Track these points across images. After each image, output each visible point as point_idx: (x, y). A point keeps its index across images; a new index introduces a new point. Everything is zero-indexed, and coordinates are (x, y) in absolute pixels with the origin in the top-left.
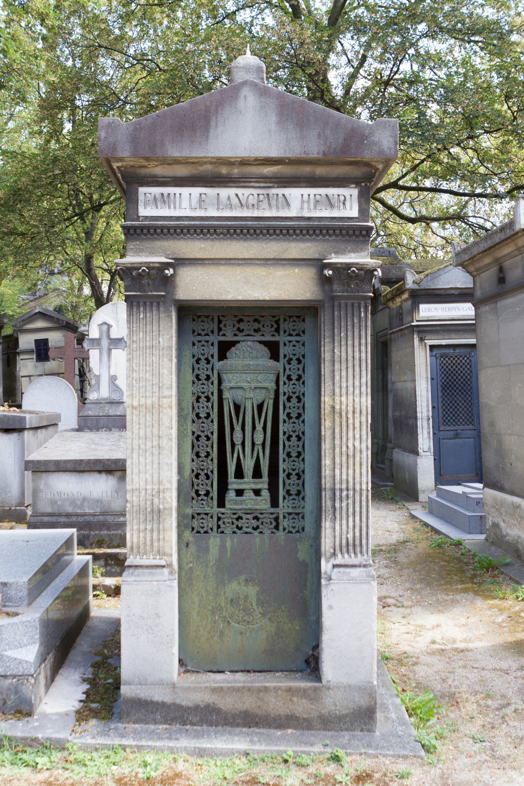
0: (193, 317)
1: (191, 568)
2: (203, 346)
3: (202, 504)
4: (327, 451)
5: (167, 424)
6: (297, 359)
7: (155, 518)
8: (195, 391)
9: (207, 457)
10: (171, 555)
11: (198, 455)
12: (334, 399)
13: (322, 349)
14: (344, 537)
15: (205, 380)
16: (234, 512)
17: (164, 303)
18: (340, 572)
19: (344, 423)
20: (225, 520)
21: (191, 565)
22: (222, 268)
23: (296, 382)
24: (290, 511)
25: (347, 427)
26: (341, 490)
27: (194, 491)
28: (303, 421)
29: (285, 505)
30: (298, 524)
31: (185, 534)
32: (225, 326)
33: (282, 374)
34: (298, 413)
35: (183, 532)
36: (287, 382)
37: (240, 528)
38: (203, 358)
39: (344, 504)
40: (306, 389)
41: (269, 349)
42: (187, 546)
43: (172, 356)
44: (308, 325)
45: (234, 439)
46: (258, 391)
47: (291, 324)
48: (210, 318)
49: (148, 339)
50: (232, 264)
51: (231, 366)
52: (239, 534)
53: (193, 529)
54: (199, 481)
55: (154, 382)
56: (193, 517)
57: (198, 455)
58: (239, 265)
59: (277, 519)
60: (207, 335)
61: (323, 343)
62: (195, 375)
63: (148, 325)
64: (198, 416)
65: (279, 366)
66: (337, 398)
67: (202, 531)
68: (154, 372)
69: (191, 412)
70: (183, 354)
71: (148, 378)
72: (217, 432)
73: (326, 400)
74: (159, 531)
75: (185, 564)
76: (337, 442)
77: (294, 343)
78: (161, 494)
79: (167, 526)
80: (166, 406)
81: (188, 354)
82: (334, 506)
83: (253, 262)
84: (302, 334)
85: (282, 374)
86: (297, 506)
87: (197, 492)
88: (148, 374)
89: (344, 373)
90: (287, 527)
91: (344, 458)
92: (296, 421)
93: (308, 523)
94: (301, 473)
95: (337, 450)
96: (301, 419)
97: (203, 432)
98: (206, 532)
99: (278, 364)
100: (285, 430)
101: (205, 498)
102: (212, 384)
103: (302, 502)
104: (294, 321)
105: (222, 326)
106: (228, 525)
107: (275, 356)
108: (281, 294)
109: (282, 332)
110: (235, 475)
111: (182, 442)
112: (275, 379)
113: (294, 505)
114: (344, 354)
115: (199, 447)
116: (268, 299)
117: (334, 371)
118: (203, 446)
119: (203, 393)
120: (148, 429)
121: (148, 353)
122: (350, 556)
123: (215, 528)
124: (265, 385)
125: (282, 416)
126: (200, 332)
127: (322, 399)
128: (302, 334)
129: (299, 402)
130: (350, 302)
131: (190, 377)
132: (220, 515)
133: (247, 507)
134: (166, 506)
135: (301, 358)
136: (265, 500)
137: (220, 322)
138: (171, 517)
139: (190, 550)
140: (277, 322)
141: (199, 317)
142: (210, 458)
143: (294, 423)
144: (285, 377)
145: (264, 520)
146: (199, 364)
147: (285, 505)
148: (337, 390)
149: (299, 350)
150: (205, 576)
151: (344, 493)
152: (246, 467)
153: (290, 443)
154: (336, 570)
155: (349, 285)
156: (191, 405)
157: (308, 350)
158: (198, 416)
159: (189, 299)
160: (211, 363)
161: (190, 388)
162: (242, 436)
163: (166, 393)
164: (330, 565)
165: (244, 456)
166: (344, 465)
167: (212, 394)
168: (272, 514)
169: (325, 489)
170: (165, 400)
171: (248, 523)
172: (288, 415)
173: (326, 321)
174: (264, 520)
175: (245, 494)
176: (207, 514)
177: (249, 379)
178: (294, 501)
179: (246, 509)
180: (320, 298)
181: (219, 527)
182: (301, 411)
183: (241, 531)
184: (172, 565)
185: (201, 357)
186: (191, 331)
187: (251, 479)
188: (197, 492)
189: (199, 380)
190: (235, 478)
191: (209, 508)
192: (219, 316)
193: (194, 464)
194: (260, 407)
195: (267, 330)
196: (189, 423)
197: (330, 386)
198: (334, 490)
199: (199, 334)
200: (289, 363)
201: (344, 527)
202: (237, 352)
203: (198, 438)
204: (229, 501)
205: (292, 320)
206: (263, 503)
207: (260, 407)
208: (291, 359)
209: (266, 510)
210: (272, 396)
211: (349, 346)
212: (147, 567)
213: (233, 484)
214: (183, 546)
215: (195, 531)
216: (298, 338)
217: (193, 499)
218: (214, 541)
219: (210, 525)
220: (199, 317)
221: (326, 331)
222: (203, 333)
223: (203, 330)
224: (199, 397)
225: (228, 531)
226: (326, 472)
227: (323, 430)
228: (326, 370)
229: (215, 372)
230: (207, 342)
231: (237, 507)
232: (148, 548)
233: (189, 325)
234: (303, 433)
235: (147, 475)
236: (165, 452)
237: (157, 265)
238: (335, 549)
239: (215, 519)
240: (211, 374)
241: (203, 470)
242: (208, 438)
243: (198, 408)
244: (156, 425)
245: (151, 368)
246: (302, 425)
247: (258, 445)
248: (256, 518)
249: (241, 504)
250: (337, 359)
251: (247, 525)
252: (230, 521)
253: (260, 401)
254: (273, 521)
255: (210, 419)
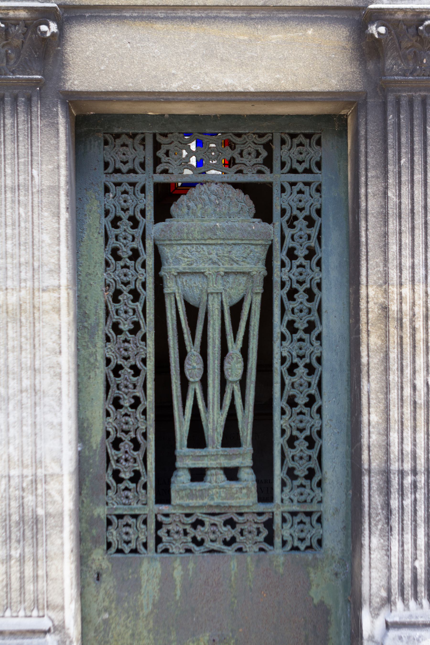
0: (103, 132)
1: (106, 622)
2: (125, 192)
3: (127, 497)
4: (372, 396)
5: (50, 344)
6: (306, 218)
7: (28, 534)
8: (110, 280)
9: (134, 406)
10: (63, 608)
11: (117, 403)
12: (386, 292)
13: (363, 191)
14: (408, 567)
15: (130, 258)
16: (188, 511)
17: (41, 98)
18: (400, 638)
19: (407, 340)
20: (170, 527)
21: (106, 616)
22: (159, 26)
23: (304, 262)
24: (295, 508)
25: (414, 347)
26: (402, 473)
27: (110, 472)
28: (319, 337)
29: (286, 498)
30: (311, 533)
31: (94, 556)
32: (167, 154)
33: (277, 246)
34: (309, 322)
35: (90, 552)
36: (287, 261)
37: (199, 543)
38: (125, 216)
39: (408, 502)
40: (323, 275)
41: (251, 198)
42: (98, 579)
43: (59, 207)
44: (327, 151)
45: (187, 373)
46: (231, 279)
47: (295, 150)
48: (139, 138)
49: (9, 171)
50: (180, 18)
51: (180, 231)
52: (197, 554)
53: (109, 545)
54: (121, 454)
55: (22, 260)
56: (109, 523)
57: (117, 403)
58: (193, 20)
59: (269, 524)
60: (133, 171)
61: (363, 179)
62: (109, 248)
63: (8, 142)
64: (116, 328)
65: (273, 231)
66: (393, 290)
67: (127, 549)
68: (23, 239)
69: (103, 320)
70: (87, 207)
71: (10, 251)
72: (153, 359)
73: (371, 293)
74: (36, 560)
75: (94, 613)
76: (394, 377)
77: (300, 186)
78: (39, 486)
79: (53, 549)
80: (47, 307)
81: (95, 206)
82: (388, 505)
83: (223, 13)
84: (315, 169)
85: (277, 246)
86: (309, 500)
87: (116, 474)
88: (9, 242)
89: (406, 239)
90: (289, 539)
91: (408, 410)
92: (306, 336)
93: (332, 532)
94: (315, 436)
95: (394, 395)
96: (315, 333)
97: (126, 358)
98: (134, 551)
99: (271, 226)
100: (285, 354)
101: (132, 486)
102: (144, 265)
103: (317, 491)
104: (301, 144)
105: (161, 154)
106: (176, 536)
107: (264, 213)
108: (278, 80)
109: (277, 165)
110: (188, 440)
111: (85, 378)
112: (264, 257)
113: (303, 498)
114: (406, 201)
115: (118, 389)
116: (252, 90)
117: (386, 235)
118: (126, 387)
119: (126, 284)
120: (11, 355)
121: (9, 200)
122: (421, 604)
123: (151, 544)
124: (246, 267)
125: (278, 327)
126: (119, 165)
127: (363, 291)
128: (315, 169)
129: (311, 299)
130: (418, 95)
131: (99, 253)
132: (160, 518)
133: (212, 503)
134: (51, 509)
135: (314, 216)
136: (247, 488)
137: (157, 146)
138: (62, 532)
139: (103, 585)
140: (268, 147)
141: (117, 136)
142: (140, 409)
143: (301, 340)
144: (285, 253)
145: (246, 527)
146: (117, 227)
147: (286, 498)
148: (393, 274)
149: (310, 201)
150: (133, 635)
151: (408, 480)
152: (210, 426)
153: (294, 379)
154: (393, 633)
155: (417, 58)
156: (103, 307)
157: (327, 200)
158: (116, 328)
159: (92, 89)
160: (141, 225)
161: (100, 275)
162: (201, 366)
163: (49, 281)
164: (380, 623)
165: (206, 405)
166: (408, 423)
167: (144, 285)
168: (260, 514)
169: (369, 471)
170: (46, 296)
171: (214, 533)
172: (291, 326)
173: (370, 135)
174: (246, 527)
175: (208, 478)
176: (135, 516)
177: (214, 256)
178: (302, 489)
179: (211, 506)
180: (358, 87)
181: (158, 540)
182: (314, 317)
183: (202, 549)
184: (64, 627)
185: (121, 214)
186: (102, 165)
187: (220, 449)
188: (116, 474)
189: (118, 258)
190: (189, 446)
191: (140, 505)
192: (155, 135)
193: (110, 420)
194: (236, 310)
195: (249, 160)
196: (100, 341)
197: (377, 265)
198: (386, 473)
199: (117, 171)
200: (292, 226)
201: (408, 546)
202: (191, 204)
203: (117, 370)
204: (178, 492)
205: (296, 141)
206: (243, 494)
207: (236, 310)
208: (295, 218)
209: (248, 507)
210: (260, 289)
211: (416, 185)
212: (13, 634)
213: (187, 458)
214: (91, 578)
215: (113, 550)
216: (308, 177)
217: (108, 487)
218: (150, 569)
219: (143, 539)
220: (117, 136)
221: (371, 154)
222: (125, 168)
223: (125, 163)
224: (117, 294)
225: (177, 548)
226: (371, 437)
227: (364, 353)
228: (370, 233)
229: (149, 244)
230: (133, 184)
231: (193, 502)
232: (15, 595)
233: (97, 152)
234: (319, 360)
235: (11, 448)
236: (47, 400)
237: (23, 14)
238: (389, 591)
239: (152, 525)
240: (141, 248)
241: (127, 432)
242: (137, 371)
243: (117, 314)
244: (27, 346)
245: (16, 231)
246: (316, 344)
247: (232, 382)
248: (230, 523)
249: (202, 497)
250: (392, 210)
251: (212, 537)
252: (181, 528)
253: (236, 299)
254: (261, 527)
255: (140, 335)
